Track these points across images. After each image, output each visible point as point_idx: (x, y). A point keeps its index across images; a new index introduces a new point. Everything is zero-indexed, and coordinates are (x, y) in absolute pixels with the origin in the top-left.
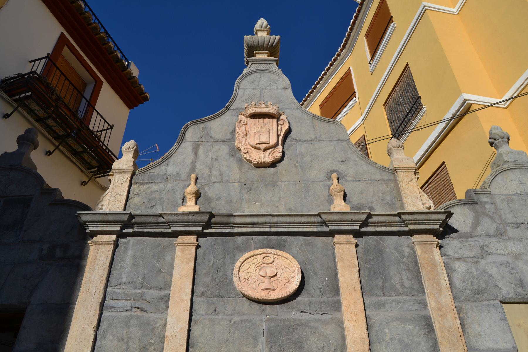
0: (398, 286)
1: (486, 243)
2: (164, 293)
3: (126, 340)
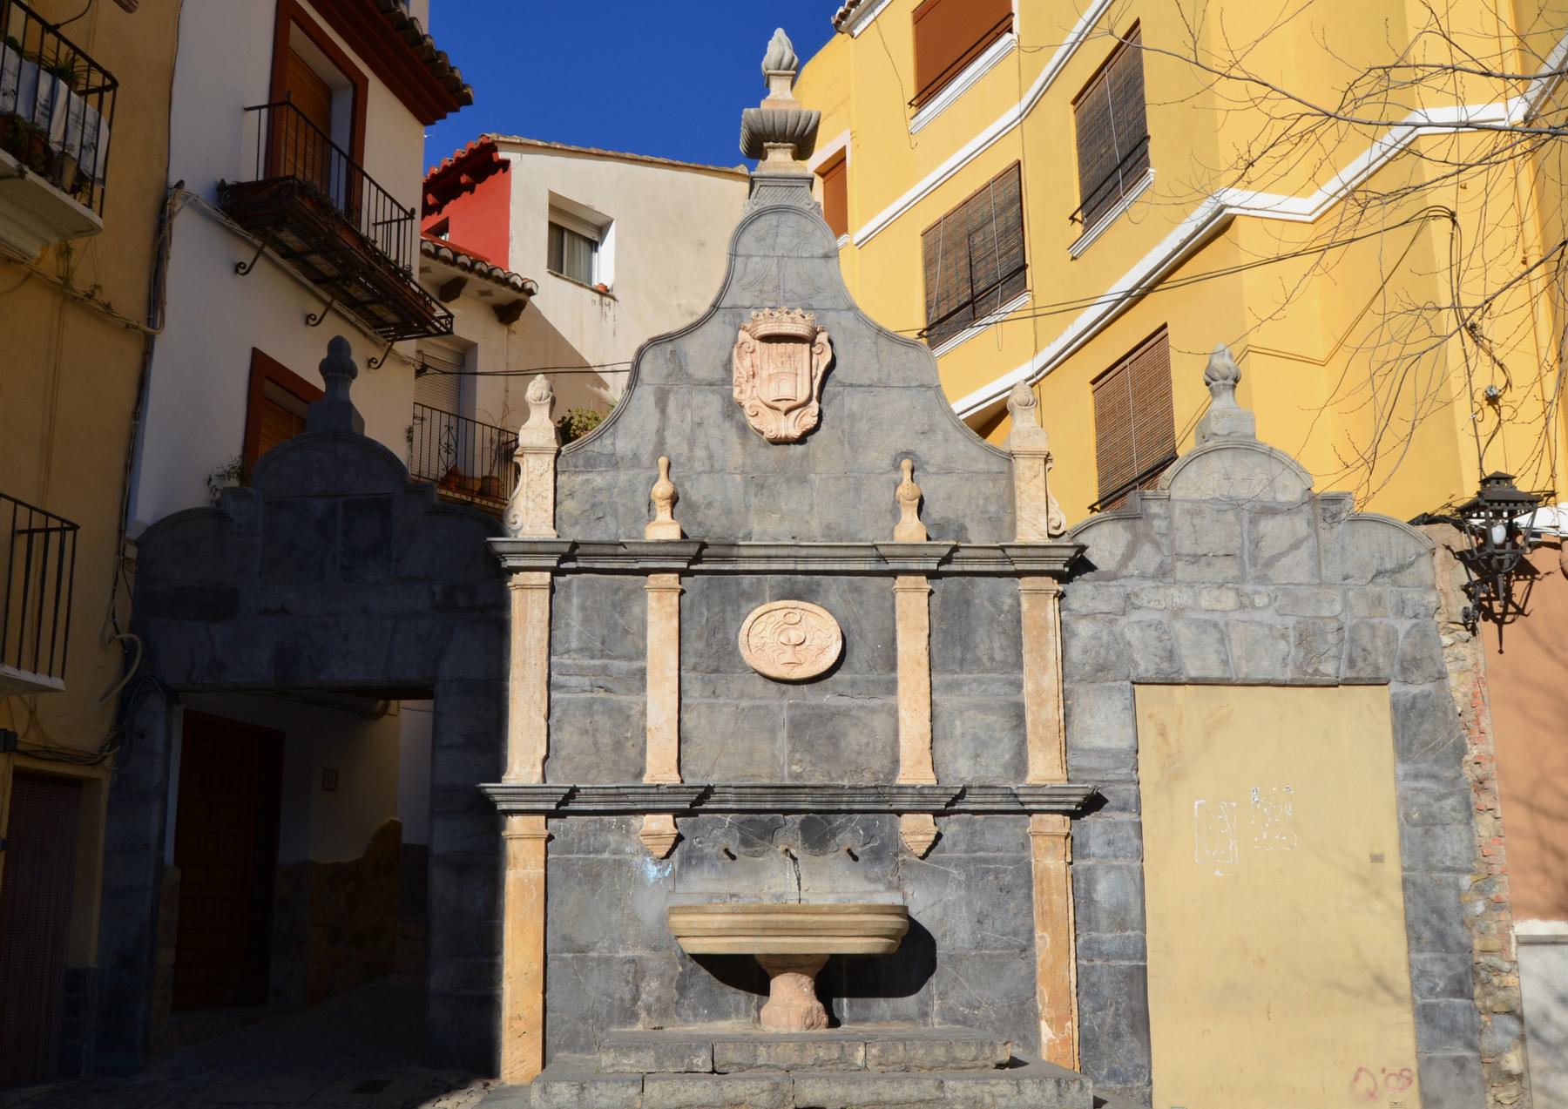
0: (985, 658)
1: (1137, 589)
2: (636, 665)
3: (591, 732)
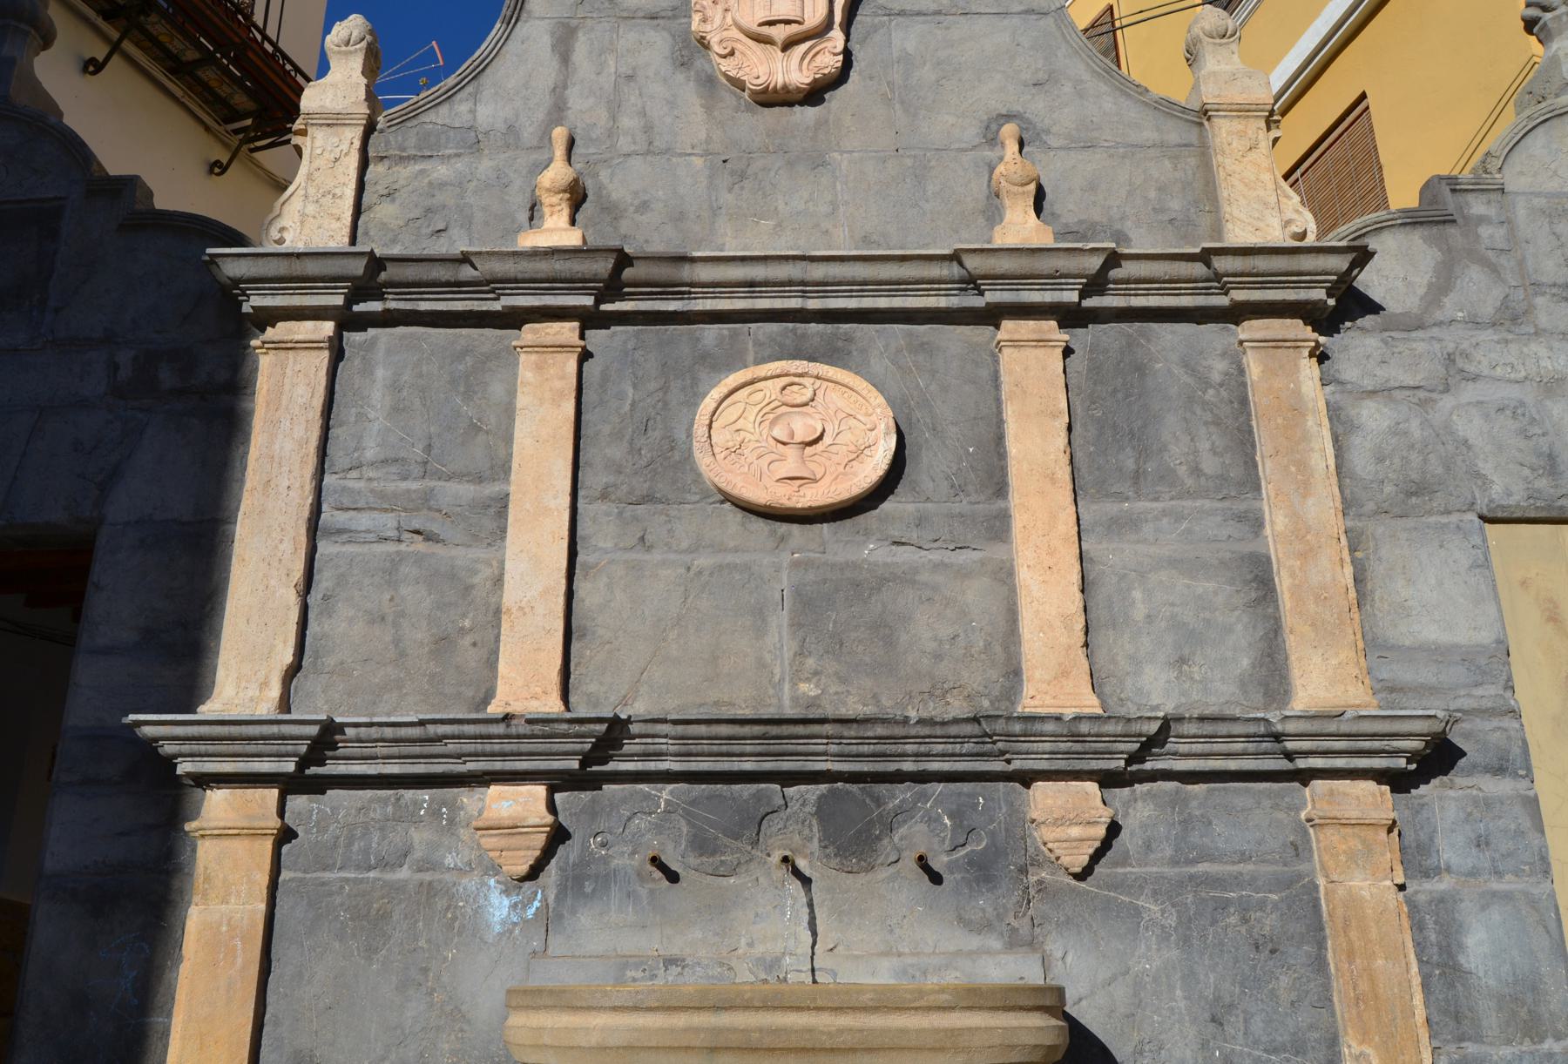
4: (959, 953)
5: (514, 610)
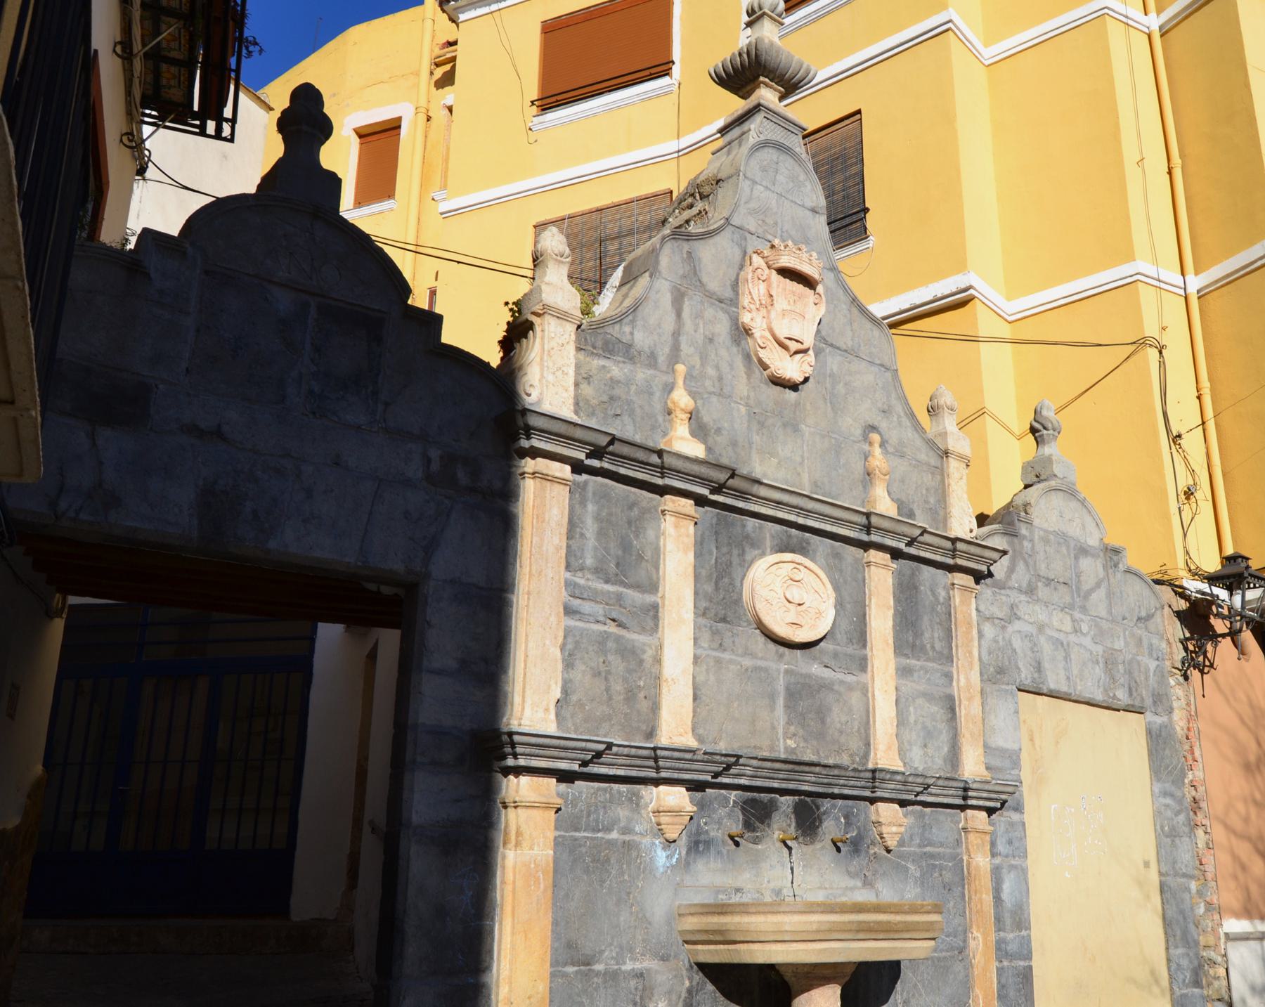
0: (928, 646)
4: (846, 888)
5: (669, 680)
